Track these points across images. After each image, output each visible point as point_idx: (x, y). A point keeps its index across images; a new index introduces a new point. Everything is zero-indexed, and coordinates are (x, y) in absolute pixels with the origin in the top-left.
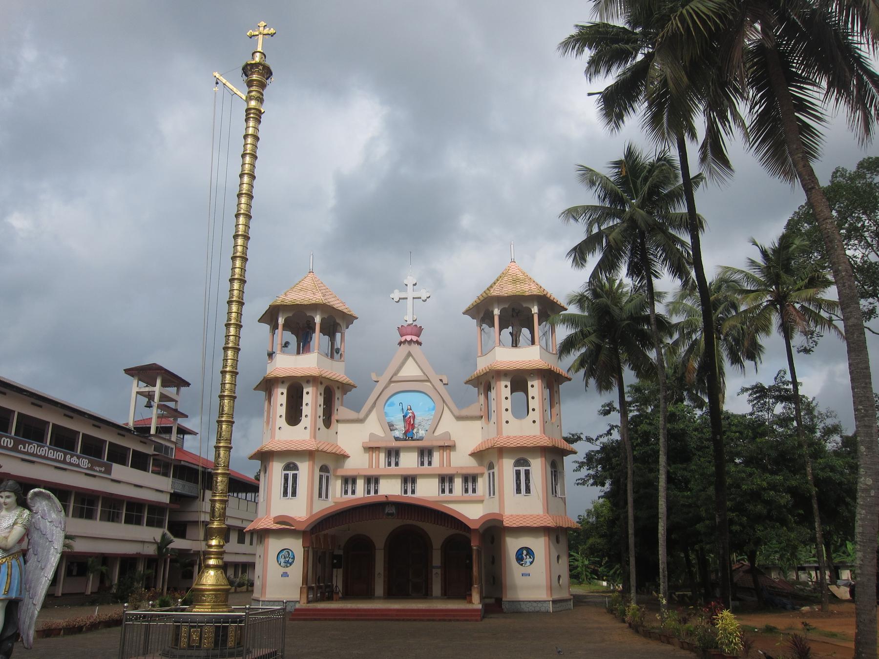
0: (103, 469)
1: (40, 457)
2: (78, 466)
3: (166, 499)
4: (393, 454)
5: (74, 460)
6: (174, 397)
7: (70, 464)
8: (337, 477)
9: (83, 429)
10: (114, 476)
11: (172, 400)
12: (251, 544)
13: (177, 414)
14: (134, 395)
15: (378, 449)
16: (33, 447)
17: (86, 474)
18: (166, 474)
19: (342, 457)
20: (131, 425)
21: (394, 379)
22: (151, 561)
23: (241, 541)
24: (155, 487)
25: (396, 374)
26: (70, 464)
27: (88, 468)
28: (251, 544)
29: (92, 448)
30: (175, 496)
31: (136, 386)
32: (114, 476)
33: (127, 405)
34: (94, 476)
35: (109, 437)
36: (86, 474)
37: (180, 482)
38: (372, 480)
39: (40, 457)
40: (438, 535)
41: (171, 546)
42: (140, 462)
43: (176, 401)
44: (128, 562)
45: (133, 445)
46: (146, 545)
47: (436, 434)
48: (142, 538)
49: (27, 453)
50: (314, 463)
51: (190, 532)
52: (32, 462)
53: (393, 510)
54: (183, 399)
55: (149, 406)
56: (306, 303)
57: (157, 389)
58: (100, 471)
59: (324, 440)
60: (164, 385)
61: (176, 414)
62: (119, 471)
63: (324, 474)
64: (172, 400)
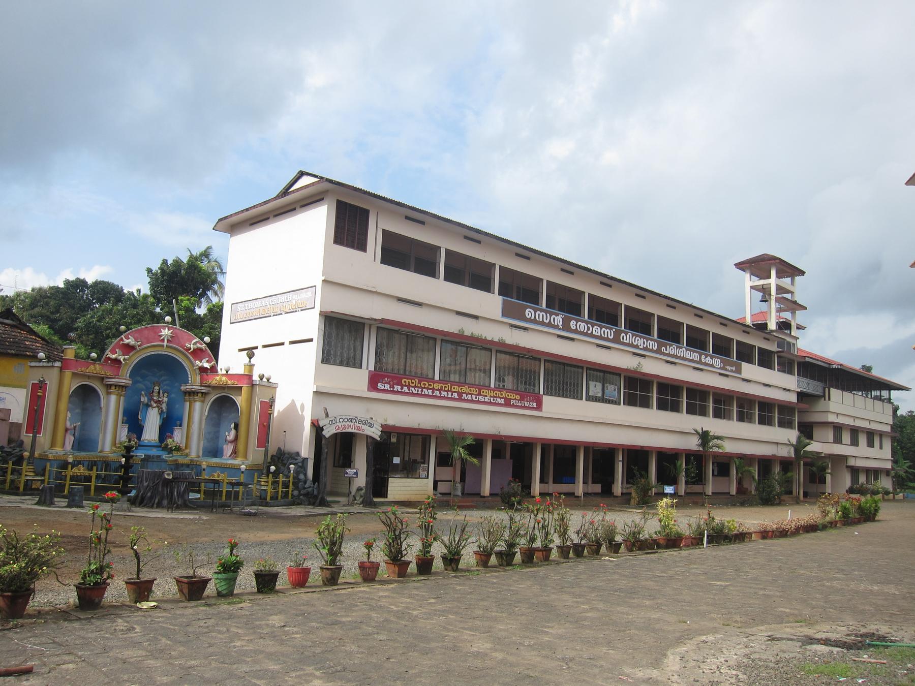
0: (734, 369)
1: (679, 358)
2: (712, 366)
3: (793, 398)
5: (708, 360)
6: (790, 288)
9: (589, 289)
10: (744, 375)
11: (788, 292)
12: (881, 448)
13: (795, 306)
14: (748, 289)
16: (672, 349)
17: (721, 374)
18: (790, 372)
20: (749, 321)
22: (786, 465)
23: (871, 444)
24: (781, 385)
26: (706, 364)
27: (720, 368)
28: (881, 448)
29: (722, 347)
30: (801, 395)
31: (748, 280)
33: (737, 299)
34: (727, 376)
35: (736, 336)
36: (721, 374)
37: (805, 380)
39: (679, 358)
41: (808, 448)
42: (765, 360)
43: (792, 293)
44: (765, 463)
45: (757, 342)
46: (780, 447)
48: (775, 440)
49: (669, 355)
51: (817, 433)
52: (573, 339)
54: (801, 290)
55: (764, 300)
57: (773, 281)
58: (732, 371)
60: (779, 276)
61: (794, 306)
62: (750, 370)
64: (788, 292)
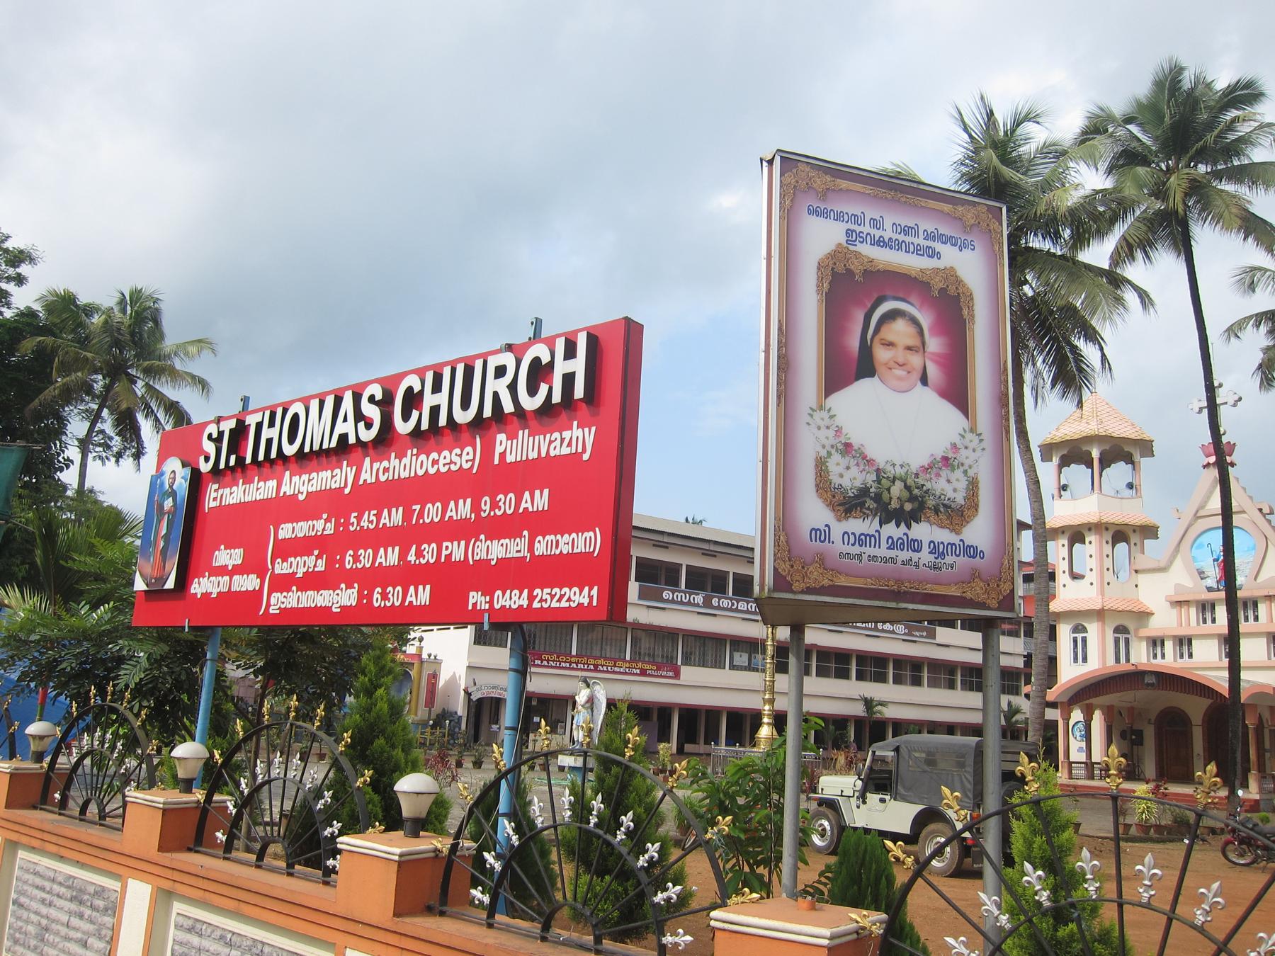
2: (893, 632)
4: (1208, 607)
7: (883, 631)
8: (1141, 638)
10: (939, 639)
15: (1187, 602)
19: (1144, 615)
21: (1201, 513)
25: (1202, 507)
26: (883, 631)
32: (939, 639)
38: (1184, 642)
40: (1196, 709)
47: (1260, 580)
50: (1104, 623)
53: (1152, 680)
56: (1077, 437)
59: (1117, 598)
62: (943, 634)
63: (1122, 637)
